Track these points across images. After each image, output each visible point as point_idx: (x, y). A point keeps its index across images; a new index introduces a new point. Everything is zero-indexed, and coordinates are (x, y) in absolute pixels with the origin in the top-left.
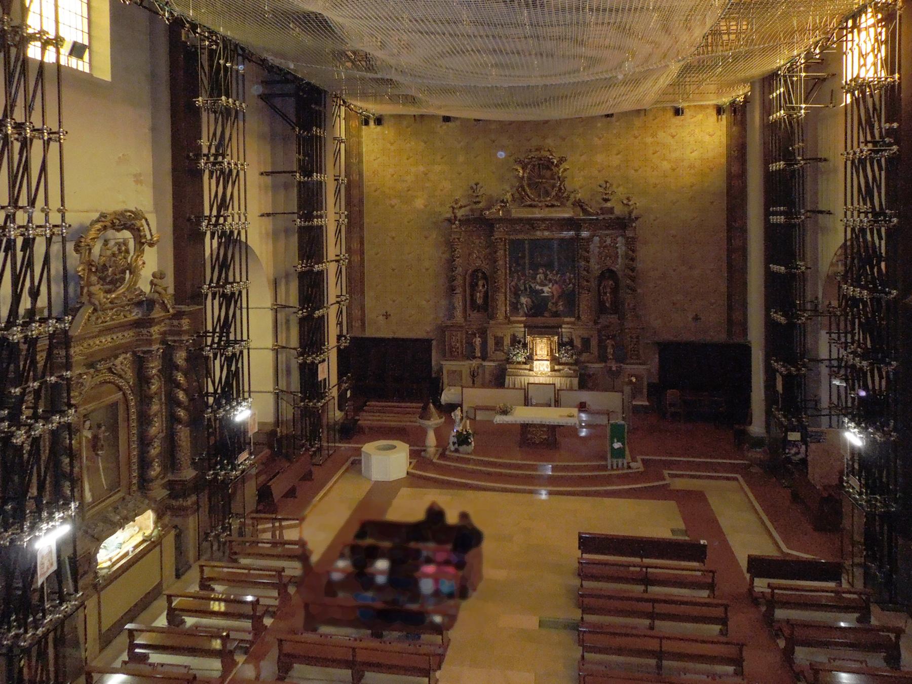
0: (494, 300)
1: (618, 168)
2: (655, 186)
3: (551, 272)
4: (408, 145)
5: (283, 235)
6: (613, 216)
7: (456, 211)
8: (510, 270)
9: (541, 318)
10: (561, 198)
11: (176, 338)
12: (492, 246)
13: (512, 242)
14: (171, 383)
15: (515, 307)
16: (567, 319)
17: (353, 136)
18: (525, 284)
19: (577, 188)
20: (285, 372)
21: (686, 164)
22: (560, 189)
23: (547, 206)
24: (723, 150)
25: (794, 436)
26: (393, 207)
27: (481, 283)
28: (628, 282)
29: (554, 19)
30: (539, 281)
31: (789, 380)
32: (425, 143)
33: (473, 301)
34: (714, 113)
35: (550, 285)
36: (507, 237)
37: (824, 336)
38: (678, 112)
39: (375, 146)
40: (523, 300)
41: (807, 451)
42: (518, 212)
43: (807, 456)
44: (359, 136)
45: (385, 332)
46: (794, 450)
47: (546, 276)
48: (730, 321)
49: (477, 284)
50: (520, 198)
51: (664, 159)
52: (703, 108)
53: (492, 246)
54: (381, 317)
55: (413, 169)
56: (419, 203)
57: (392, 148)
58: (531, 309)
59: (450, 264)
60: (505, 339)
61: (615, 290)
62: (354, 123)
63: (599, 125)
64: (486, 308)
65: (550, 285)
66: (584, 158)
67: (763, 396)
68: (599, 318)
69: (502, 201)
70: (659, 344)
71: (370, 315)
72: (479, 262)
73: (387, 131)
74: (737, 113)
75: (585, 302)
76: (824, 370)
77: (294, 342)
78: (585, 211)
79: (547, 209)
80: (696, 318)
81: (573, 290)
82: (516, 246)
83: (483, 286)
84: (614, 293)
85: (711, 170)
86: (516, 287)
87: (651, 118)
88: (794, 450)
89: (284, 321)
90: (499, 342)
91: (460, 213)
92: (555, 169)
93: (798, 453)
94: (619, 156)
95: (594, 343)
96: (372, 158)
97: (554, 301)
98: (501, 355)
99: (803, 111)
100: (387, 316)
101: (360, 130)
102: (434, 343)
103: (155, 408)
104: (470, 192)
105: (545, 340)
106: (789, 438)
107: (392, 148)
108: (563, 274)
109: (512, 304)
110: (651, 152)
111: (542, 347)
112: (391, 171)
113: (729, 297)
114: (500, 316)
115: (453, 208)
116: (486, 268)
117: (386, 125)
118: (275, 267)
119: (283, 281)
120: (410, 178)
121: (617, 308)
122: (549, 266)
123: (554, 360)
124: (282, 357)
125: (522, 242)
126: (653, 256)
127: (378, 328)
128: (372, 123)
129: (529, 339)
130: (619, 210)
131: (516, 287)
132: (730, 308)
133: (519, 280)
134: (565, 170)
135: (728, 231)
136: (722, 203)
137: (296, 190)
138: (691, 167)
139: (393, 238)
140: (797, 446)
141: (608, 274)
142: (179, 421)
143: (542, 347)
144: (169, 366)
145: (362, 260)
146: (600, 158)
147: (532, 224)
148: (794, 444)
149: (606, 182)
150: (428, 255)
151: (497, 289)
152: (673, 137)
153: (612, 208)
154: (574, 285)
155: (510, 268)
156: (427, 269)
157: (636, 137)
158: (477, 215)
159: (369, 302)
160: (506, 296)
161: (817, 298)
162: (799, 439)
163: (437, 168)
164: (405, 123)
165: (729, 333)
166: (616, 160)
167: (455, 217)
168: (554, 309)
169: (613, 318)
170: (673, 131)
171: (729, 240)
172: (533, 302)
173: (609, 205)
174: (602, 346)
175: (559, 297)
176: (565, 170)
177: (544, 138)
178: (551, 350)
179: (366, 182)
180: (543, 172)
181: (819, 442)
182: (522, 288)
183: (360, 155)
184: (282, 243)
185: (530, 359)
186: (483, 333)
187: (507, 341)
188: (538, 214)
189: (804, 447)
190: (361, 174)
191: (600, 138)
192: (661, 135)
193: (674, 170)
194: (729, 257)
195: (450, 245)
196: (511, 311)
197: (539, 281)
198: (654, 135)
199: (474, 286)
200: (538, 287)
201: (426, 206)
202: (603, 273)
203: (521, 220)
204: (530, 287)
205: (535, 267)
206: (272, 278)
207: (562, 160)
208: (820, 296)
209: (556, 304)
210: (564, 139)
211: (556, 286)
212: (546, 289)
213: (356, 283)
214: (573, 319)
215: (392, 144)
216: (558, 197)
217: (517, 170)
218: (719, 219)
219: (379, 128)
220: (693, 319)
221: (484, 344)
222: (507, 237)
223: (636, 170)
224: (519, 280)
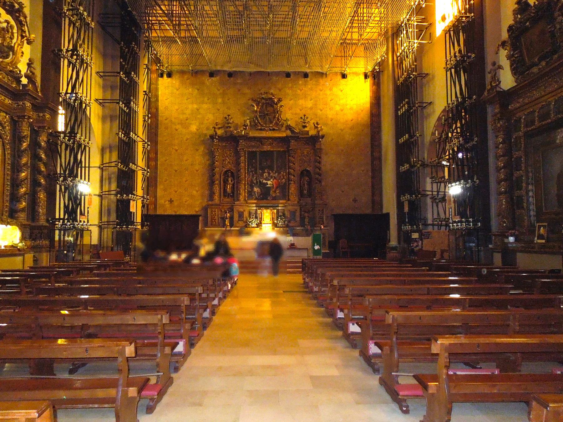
0: (238, 189)
1: (311, 108)
2: (332, 120)
3: (273, 172)
4: (188, 91)
5: (109, 120)
6: (307, 136)
7: (217, 130)
8: (248, 171)
9: (265, 198)
10: (278, 125)
11: (41, 125)
12: (237, 154)
13: (249, 153)
14: (35, 157)
15: (250, 194)
16: (281, 201)
17: (153, 84)
18: (256, 179)
19: (288, 118)
20: (106, 211)
21: (348, 107)
22: (278, 119)
23: (270, 130)
24: (368, 105)
25: (415, 236)
26: (177, 130)
27: (230, 180)
28: (317, 176)
29: (277, 20)
30: (265, 177)
31: (411, 203)
32: (198, 90)
33: (225, 191)
34: (363, 77)
35: (272, 180)
36: (246, 149)
37: (429, 180)
38: (344, 76)
39: (166, 89)
40: (256, 189)
41: (422, 244)
42: (252, 134)
43: (422, 247)
44: (157, 84)
45: (169, 212)
46: (415, 244)
47: (269, 173)
48: (373, 202)
49: (228, 180)
50: (254, 126)
51: (336, 104)
52: (356, 74)
53: (237, 154)
54: (167, 202)
55: (190, 106)
56: (194, 128)
57: (178, 92)
58: (261, 195)
59: (212, 168)
60: (245, 213)
61: (310, 184)
62: (154, 76)
63: (300, 82)
64: (234, 195)
65: (272, 180)
66: (291, 102)
67: (396, 222)
68: (300, 200)
69: (244, 125)
70: (334, 215)
71: (160, 201)
72: (229, 165)
73: (175, 81)
74: (375, 76)
75: (293, 189)
76: (429, 201)
77: (114, 186)
78: (292, 132)
79: (270, 132)
80: (355, 200)
81: (285, 183)
82: (252, 155)
83: (232, 181)
84: (310, 183)
85: (362, 111)
86: (252, 181)
87: (329, 79)
88: (415, 244)
89: (107, 177)
90: (241, 215)
91: (219, 132)
92: (275, 106)
93: (417, 246)
94: (312, 101)
95: (298, 214)
96: (165, 98)
97: (274, 190)
98: (241, 224)
99: (416, 45)
100: (171, 201)
101: (157, 80)
102: (201, 218)
103: (24, 160)
104: (225, 120)
105: (269, 211)
106: (413, 237)
107: (178, 92)
108: (279, 173)
109: (249, 192)
110: (329, 99)
111: (267, 215)
112: (176, 107)
113: (373, 186)
114: (242, 198)
115: (215, 128)
116: (234, 169)
117: (174, 77)
118: (103, 140)
119: (108, 151)
120: (188, 112)
121: (310, 194)
122: (271, 168)
123: (275, 225)
124: (105, 202)
125: (256, 152)
126: (330, 161)
127: (165, 208)
128: (165, 76)
129: (259, 211)
130: (312, 132)
131: (252, 181)
132: (373, 194)
133: (253, 176)
134: (281, 106)
135: (372, 147)
136: (368, 131)
137: (118, 91)
138: (351, 109)
139: (177, 150)
140: (417, 241)
141: (304, 173)
142: (40, 184)
143: (267, 215)
144: (35, 144)
145: (156, 165)
146: (301, 102)
147: (260, 140)
148: (415, 240)
149: (305, 116)
150: (197, 160)
151: (239, 182)
152: (342, 91)
153: (308, 132)
154: (286, 180)
155: (248, 169)
156: (197, 171)
157: (321, 91)
158: (228, 134)
159: (160, 193)
160: (245, 186)
161: (424, 159)
162: (418, 237)
163: (205, 106)
164: (186, 77)
165: (373, 208)
166: (310, 104)
167: (216, 133)
168: (274, 195)
169: (309, 200)
170: (341, 87)
171: (372, 152)
172: (261, 190)
173: (306, 129)
174: (302, 218)
175: (277, 188)
176: (281, 106)
177: (270, 88)
178: (273, 218)
179: (160, 113)
180: (269, 109)
181: (428, 238)
182: (255, 182)
183: (157, 97)
184: (108, 125)
185: (259, 225)
186: (231, 210)
187: (246, 214)
188: (264, 134)
189: (420, 242)
190: (157, 109)
191: (301, 90)
192: (335, 89)
193: (342, 110)
194: (372, 162)
195: (211, 154)
196: (248, 197)
197: (265, 177)
198: (331, 89)
199: (225, 182)
200: (264, 181)
201: (197, 130)
202: (302, 172)
203: (254, 138)
204: (260, 181)
205: (263, 169)
206: (100, 147)
207: (280, 100)
208: (426, 158)
209: (275, 192)
210: (280, 90)
211: (275, 180)
212: (269, 182)
213: (151, 183)
214: (285, 201)
215: (177, 90)
216: (277, 124)
217: (253, 106)
218: (368, 140)
219: (169, 79)
220: (353, 200)
221: (231, 218)
222: (246, 149)
223: (321, 110)
224: (253, 176)
